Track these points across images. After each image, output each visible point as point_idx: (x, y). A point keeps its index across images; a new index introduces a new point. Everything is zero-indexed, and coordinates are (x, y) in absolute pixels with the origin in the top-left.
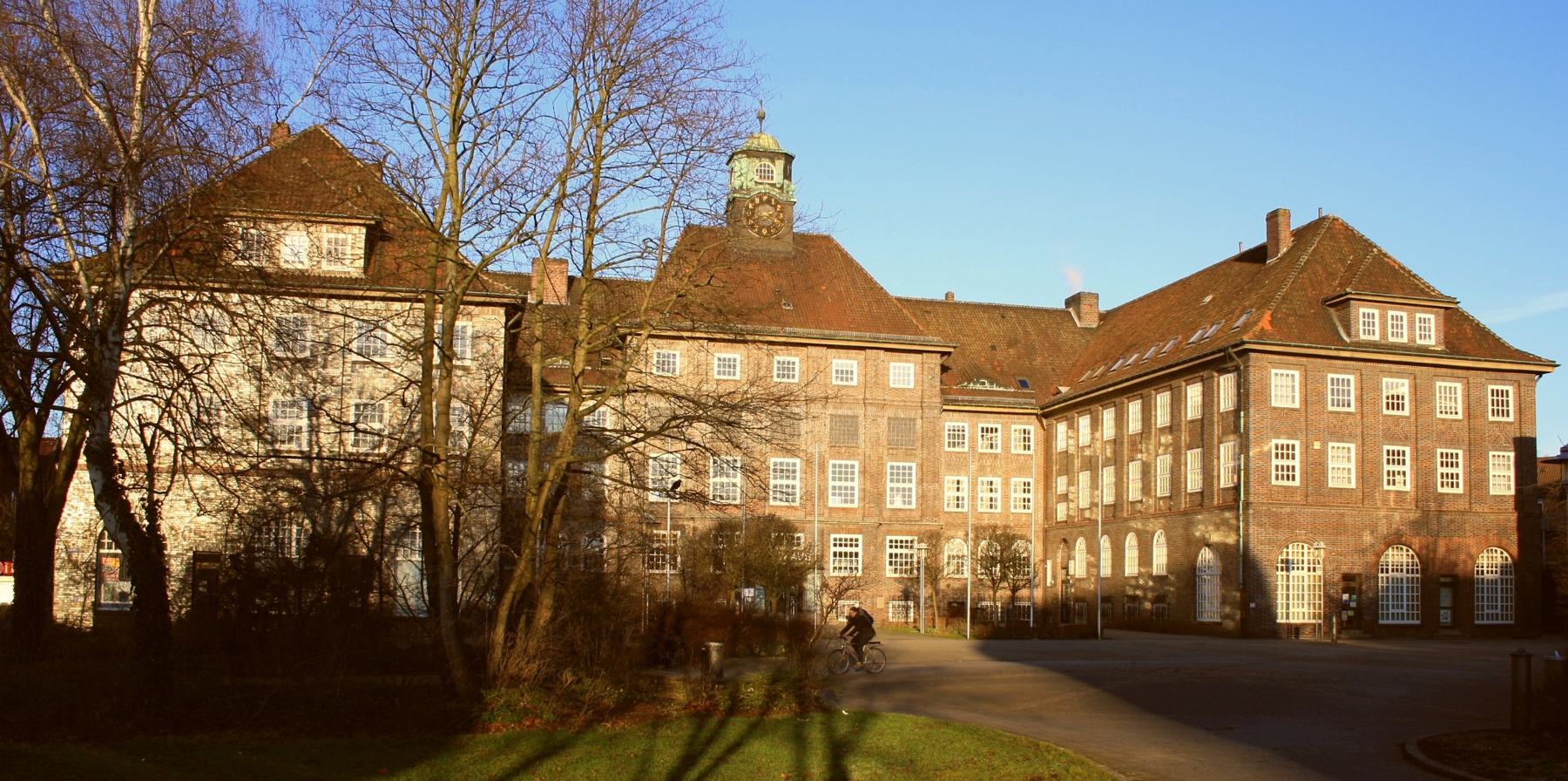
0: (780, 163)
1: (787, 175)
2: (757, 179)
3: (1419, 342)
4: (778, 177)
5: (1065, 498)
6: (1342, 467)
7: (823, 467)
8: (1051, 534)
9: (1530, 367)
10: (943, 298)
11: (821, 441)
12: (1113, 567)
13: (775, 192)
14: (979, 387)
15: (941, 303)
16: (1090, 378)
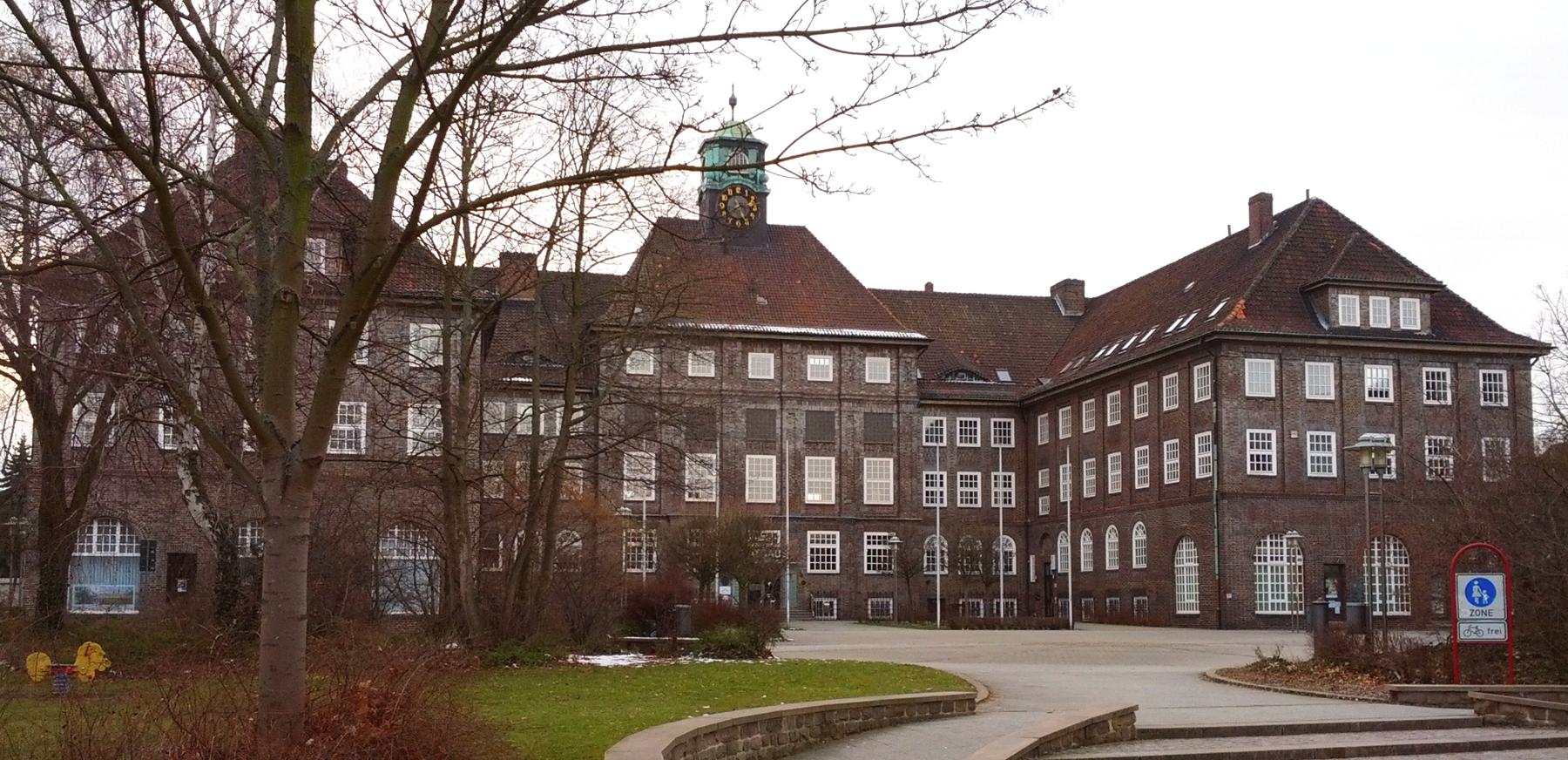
10: (923, 289)
16: (1071, 369)
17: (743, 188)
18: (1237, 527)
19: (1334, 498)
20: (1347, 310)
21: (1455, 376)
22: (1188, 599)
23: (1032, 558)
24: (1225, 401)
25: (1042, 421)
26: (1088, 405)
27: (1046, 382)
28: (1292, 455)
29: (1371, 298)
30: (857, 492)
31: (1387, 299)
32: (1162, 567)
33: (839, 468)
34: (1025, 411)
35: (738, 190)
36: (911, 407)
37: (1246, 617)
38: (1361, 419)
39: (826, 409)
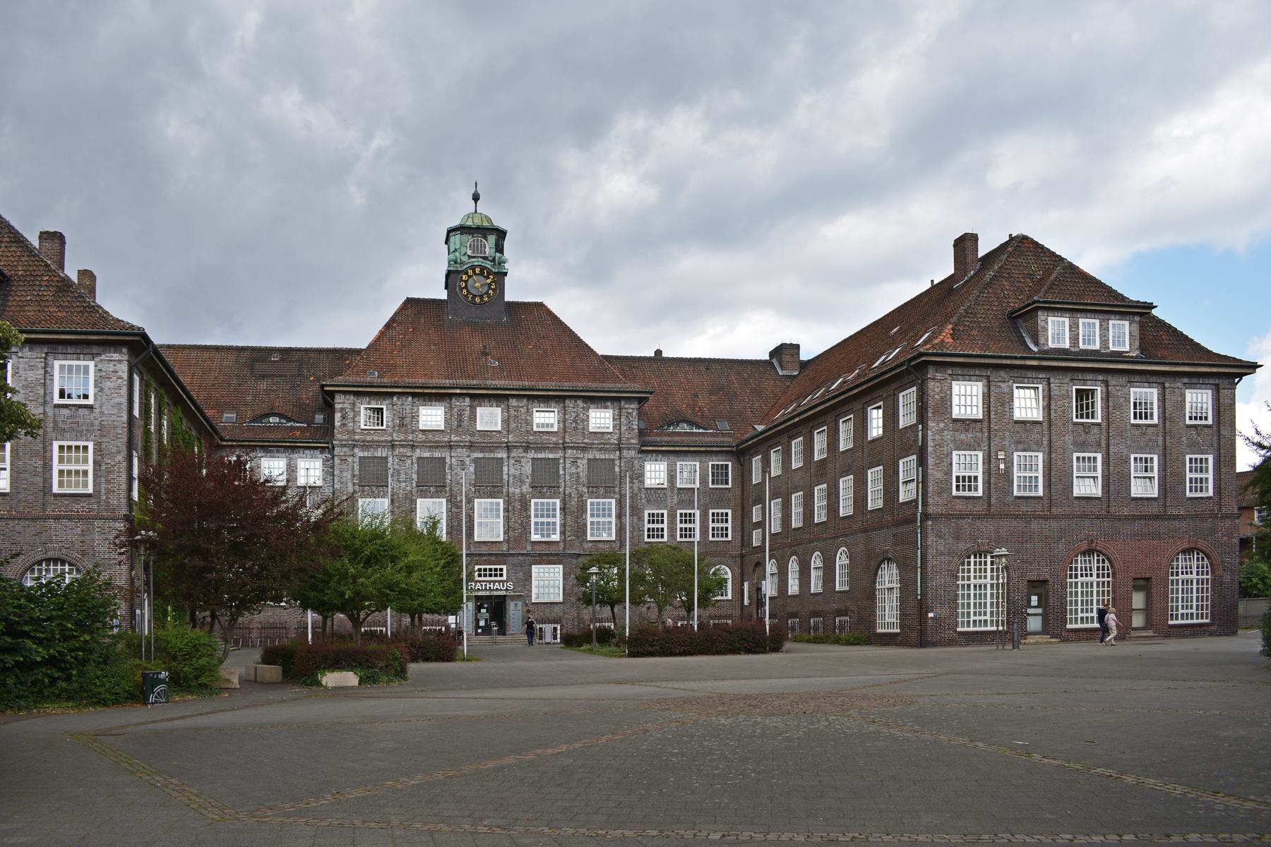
0: (492, 239)
2: (469, 252)
4: (489, 250)
5: (761, 525)
6: (1028, 473)
7: (525, 507)
8: (747, 559)
9: (1227, 373)
11: (522, 482)
12: (801, 585)
14: (679, 430)
17: (483, 268)
18: (941, 548)
19: (1040, 517)
20: (1057, 331)
21: (1162, 400)
22: (888, 616)
23: (746, 584)
24: (931, 424)
25: (756, 462)
26: (797, 444)
27: (760, 428)
29: (1081, 321)
30: (581, 530)
31: (1097, 322)
32: (865, 594)
33: (563, 510)
34: (741, 454)
35: (478, 270)
36: (633, 453)
37: (948, 634)
38: (1068, 438)
39: (551, 456)
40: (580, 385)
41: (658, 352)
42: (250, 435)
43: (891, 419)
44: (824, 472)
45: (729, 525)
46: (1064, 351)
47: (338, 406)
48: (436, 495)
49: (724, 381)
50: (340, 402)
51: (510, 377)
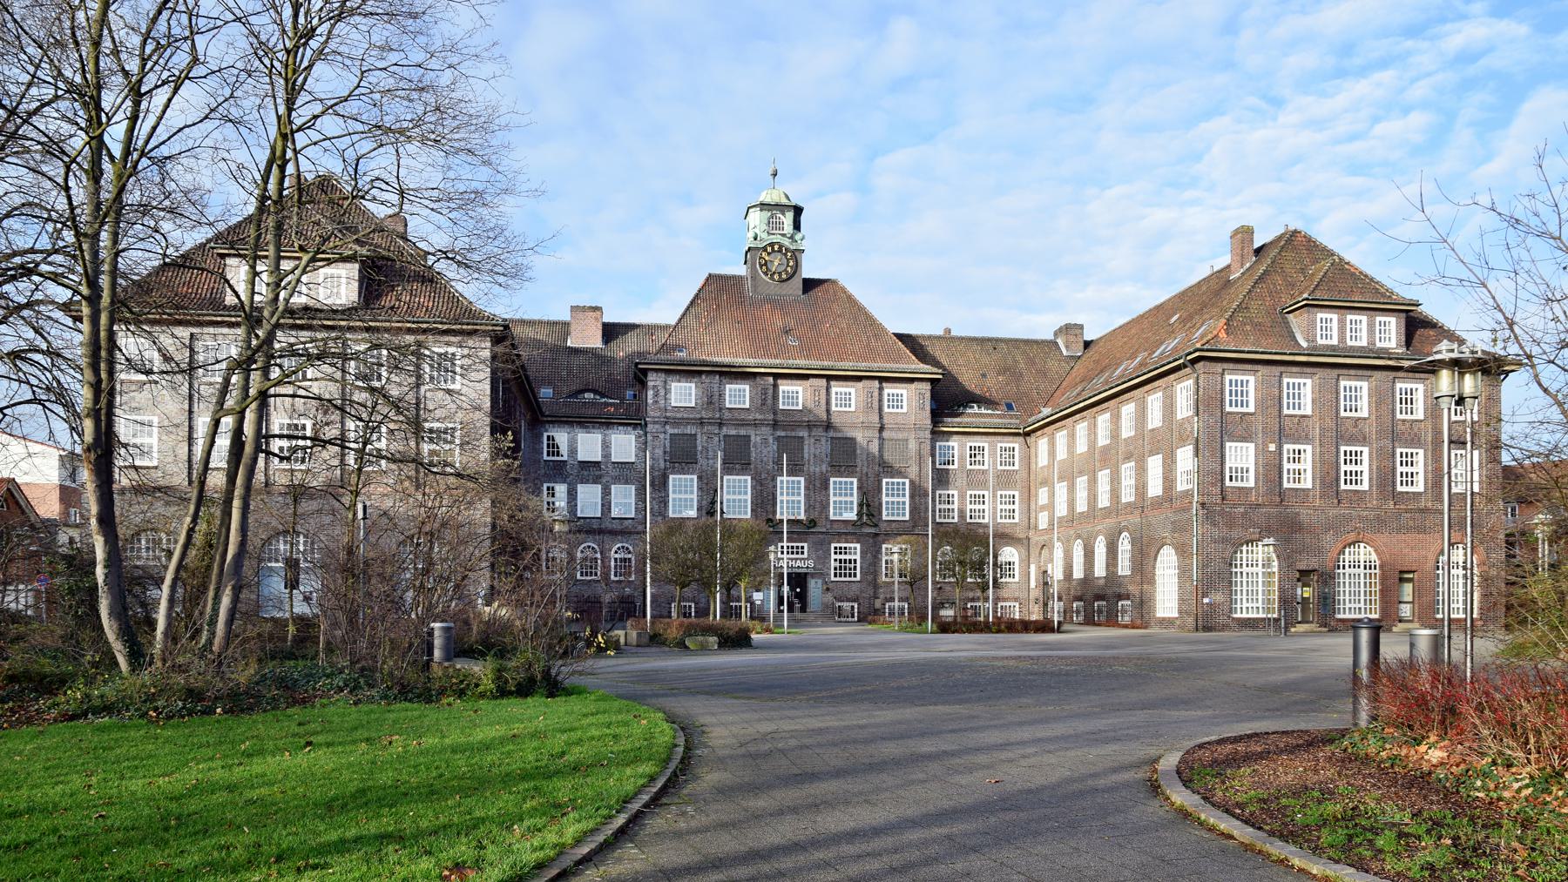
0: (790, 215)
1: (797, 226)
3: (1379, 345)
10: (941, 333)
13: (786, 242)
15: (939, 338)
28: (1272, 470)
40: (875, 365)
41: (948, 331)
42: (569, 411)
43: (1169, 407)
44: (1107, 457)
45: (1016, 507)
46: (1332, 348)
47: (650, 384)
48: (742, 472)
49: (1010, 361)
50: (653, 380)
51: (808, 357)
